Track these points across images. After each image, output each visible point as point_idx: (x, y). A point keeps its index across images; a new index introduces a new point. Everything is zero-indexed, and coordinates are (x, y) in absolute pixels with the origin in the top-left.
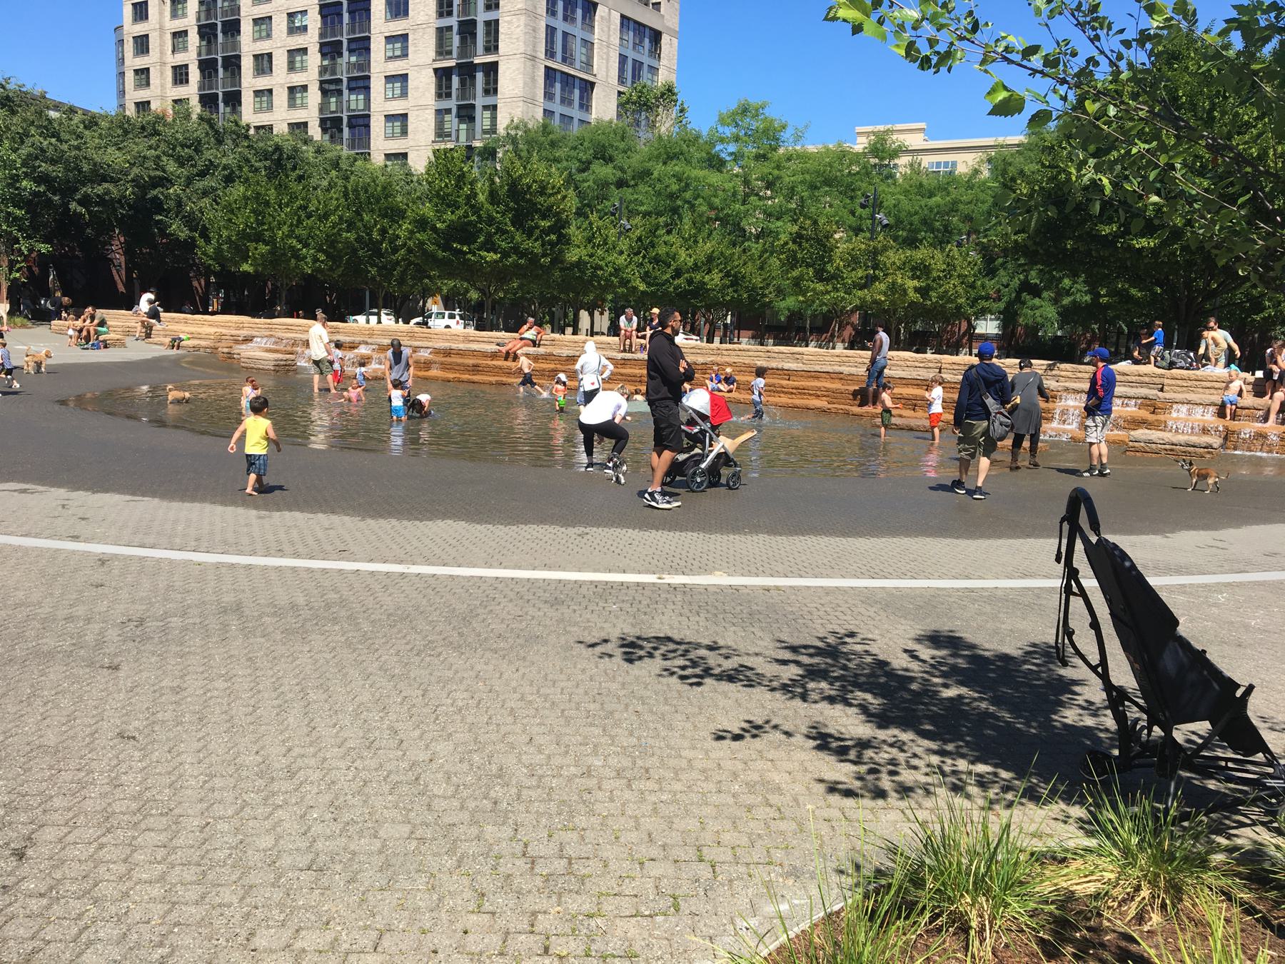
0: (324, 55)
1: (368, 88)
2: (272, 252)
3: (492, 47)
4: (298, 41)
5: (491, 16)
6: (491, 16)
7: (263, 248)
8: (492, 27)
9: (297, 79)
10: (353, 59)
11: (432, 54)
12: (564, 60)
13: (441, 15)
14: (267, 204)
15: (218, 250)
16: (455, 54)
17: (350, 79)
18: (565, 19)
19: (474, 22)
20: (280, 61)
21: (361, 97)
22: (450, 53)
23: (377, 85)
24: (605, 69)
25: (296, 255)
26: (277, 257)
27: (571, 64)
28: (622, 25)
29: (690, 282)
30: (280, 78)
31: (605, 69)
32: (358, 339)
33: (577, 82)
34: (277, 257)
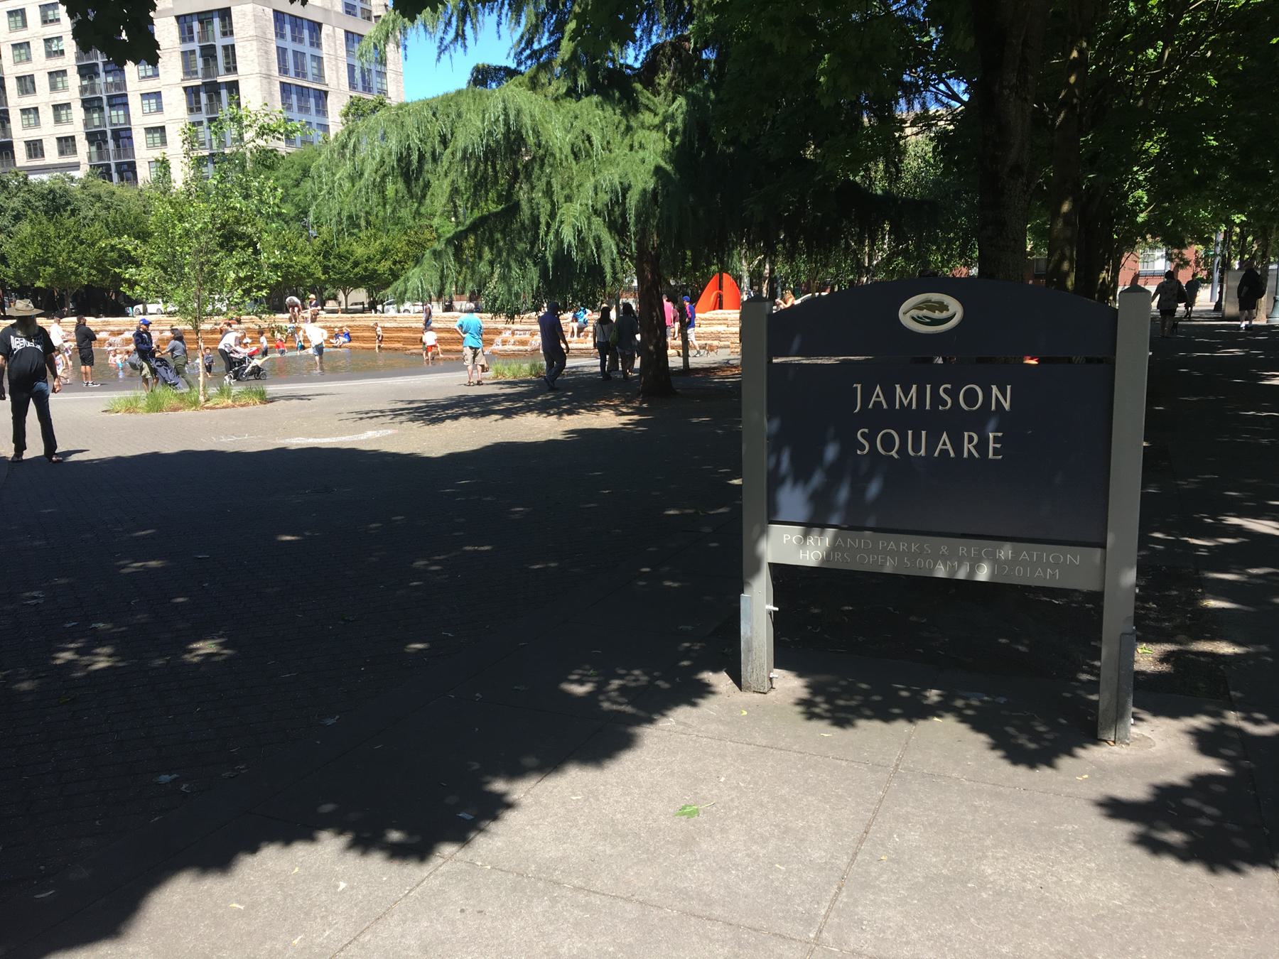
0: (82, 77)
1: (126, 105)
2: (57, 272)
3: (231, 68)
4: (56, 64)
5: (227, 41)
6: (227, 41)
7: (50, 270)
8: (230, 50)
9: (61, 98)
10: (110, 79)
11: (181, 75)
12: (297, 75)
13: (183, 40)
14: (49, 238)
15: (17, 273)
16: (200, 75)
17: (110, 98)
18: (294, 39)
19: (213, 47)
20: (42, 82)
21: (121, 112)
22: (196, 73)
23: (134, 102)
24: (336, 80)
25: (74, 272)
26: (61, 275)
27: (304, 76)
28: (347, 39)
29: (366, 269)
30: (43, 97)
31: (336, 80)
32: (123, 328)
33: (311, 92)
34: (61, 275)
